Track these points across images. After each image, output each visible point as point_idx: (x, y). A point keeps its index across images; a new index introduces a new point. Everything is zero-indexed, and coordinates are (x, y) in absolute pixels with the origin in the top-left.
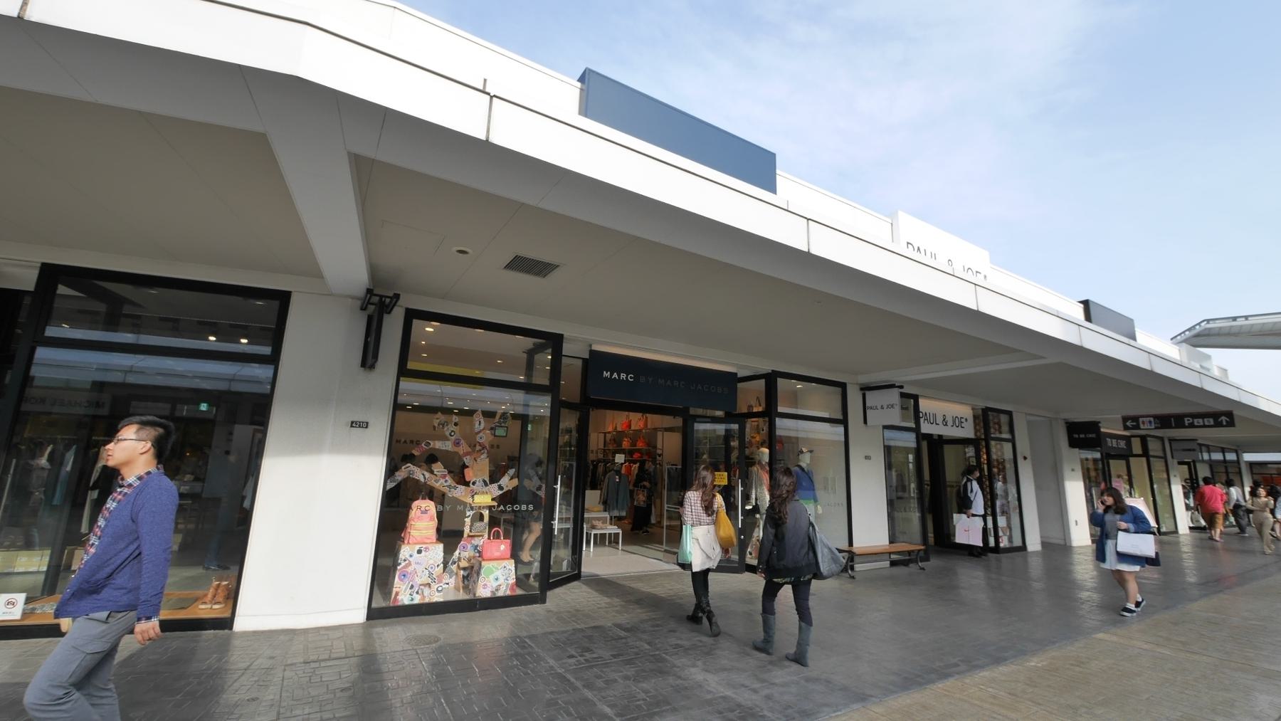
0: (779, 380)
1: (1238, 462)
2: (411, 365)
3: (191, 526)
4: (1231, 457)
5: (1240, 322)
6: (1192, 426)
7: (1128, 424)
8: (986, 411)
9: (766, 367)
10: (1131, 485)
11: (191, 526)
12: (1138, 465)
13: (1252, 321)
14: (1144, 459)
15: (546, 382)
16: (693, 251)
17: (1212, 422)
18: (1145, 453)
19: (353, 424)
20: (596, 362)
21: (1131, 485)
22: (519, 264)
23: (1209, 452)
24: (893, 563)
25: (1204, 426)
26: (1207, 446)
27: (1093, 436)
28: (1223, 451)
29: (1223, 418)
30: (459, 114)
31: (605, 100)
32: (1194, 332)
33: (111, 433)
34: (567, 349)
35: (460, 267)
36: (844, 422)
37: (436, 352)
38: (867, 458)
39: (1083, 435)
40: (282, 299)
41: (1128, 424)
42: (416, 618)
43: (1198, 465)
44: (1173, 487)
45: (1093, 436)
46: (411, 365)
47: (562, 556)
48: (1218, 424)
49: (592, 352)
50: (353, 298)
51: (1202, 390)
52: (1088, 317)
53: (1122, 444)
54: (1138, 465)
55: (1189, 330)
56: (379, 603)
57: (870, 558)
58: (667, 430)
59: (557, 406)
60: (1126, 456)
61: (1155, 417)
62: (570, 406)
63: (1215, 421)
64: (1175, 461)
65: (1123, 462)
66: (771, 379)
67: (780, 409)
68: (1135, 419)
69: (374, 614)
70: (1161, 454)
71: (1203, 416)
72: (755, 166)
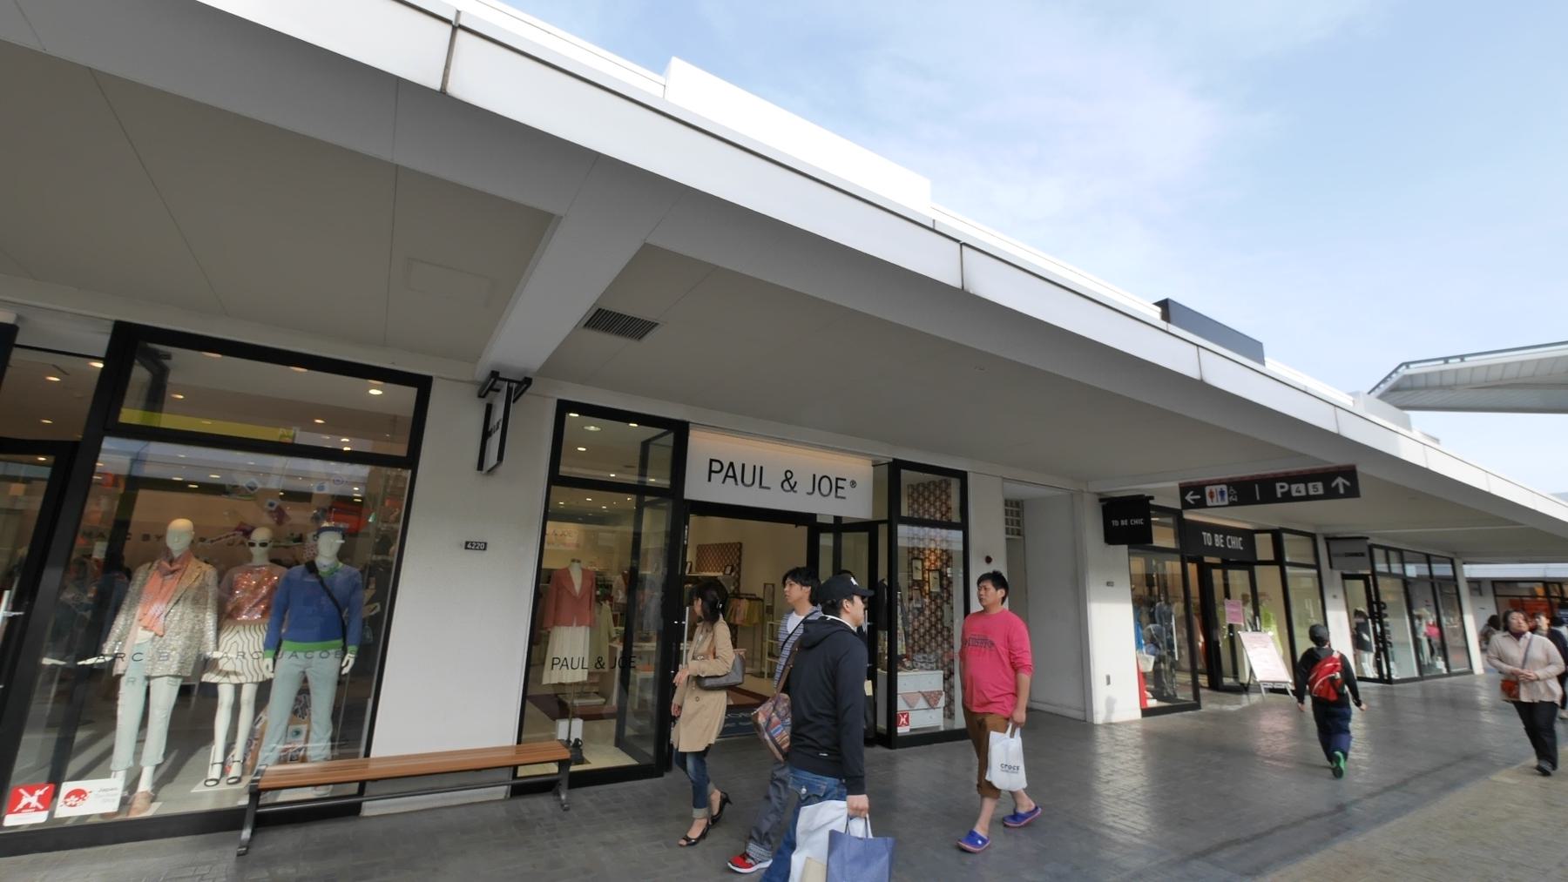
0: (903, 472)
1: (1455, 578)
2: (564, 470)
4: (1442, 570)
5: (1455, 364)
6: (1288, 498)
7: (1189, 498)
8: (896, 467)
9: (1276, 525)
10: (1257, 613)
12: (1268, 578)
13: (1470, 362)
14: (1276, 568)
15: (1271, 557)
16: (758, 275)
17: (1319, 488)
18: (1279, 560)
19: (468, 545)
21: (1257, 613)
23: (1403, 562)
24: (522, 789)
25: (1308, 498)
26: (1400, 552)
27: (1115, 523)
28: (1429, 560)
29: (1340, 481)
30: (1331, 427)
32: (1390, 383)
36: (1317, 566)
37: (201, 401)
38: (1109, 584)
39: (1126, 520)
40: (423, 384)
41: (1189, 498)
43: (1380, 580)
44: (1330, 614)
45: (1115, 523)
46: (564, 470)
48: (1331, 493)
50: (473, 382)
51: (438, 107)
52: (1166, 317)
53: (1236, 543)
54: (1268, 578)
55: (1384, 381)
57: (463, 779)
58: (637, 537)
60: (1247, 562)
61: (1231, 483)
63: (1326, 487)
64: (1337, 574)
65: (1245, 574)
67: (1288, 559)
68: (1199, 488)
70: (1311, 561)
71: (1305, 478)
72: (1251, 349)
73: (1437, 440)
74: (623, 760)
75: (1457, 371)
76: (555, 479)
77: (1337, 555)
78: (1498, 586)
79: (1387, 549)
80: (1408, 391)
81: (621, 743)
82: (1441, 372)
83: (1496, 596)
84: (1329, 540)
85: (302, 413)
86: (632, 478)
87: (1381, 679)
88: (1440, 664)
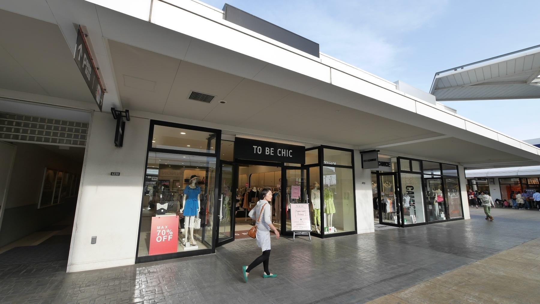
0: (324, 149)
1: (458, 178)
3: (448, 190)
9: (319, 144)
11: (448, 190)
19: (112, 174)
20: (242, 145)
22: (195, 96)
26: (421, 162)
28: (441, 167)
30: (326, 79)
31: (231, 13)
33: (337, 180)
34: (223, 137)
35: (170, 97)
36: (353, 167)
38: (363, 183)
42: (147, 263)
44: (462, 193)
47: (224, 230)
49: (236, 138)
56: (143, 254)
59: (220, 163)
62: (228, 163)
64: (368, 171)
66: (321, 149)
67: (325, 162)
69: (139, 260)
73: (455, 111)
74: (203, 247)
75: (460, 73)
76: (150, 149)
77: (365, 161)
78: (502, 181)
79: (411, 160)
80: (443, 89)
81: (203, 242)
82: (453, 75)
83: (500, 184)
84: (363, 153)
85: (183, 141)
86: (205, 151)
87: (398, 225)
88: (443, 216)
